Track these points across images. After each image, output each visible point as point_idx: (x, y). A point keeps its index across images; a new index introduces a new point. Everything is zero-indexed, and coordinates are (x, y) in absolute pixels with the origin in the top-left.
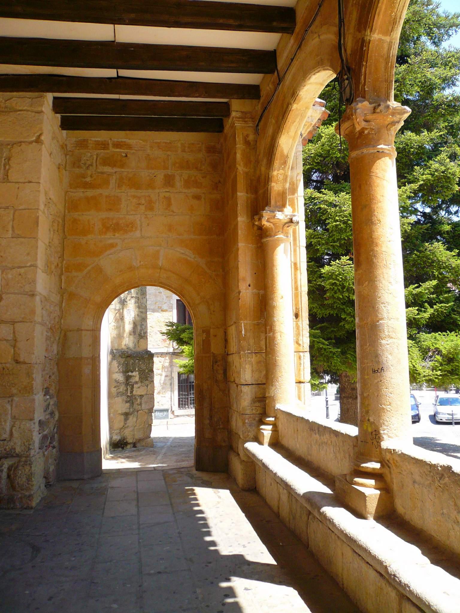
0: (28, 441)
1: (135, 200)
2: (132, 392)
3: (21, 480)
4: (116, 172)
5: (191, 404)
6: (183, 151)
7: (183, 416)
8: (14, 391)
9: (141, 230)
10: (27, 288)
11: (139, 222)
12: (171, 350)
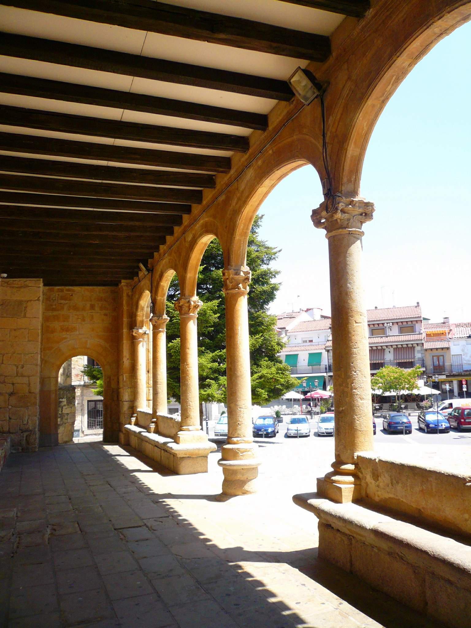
1: (76, 317)
4: (67, 303)
5: (97, 425)
7: (91, 435)
8: (29, 404)
9: (79, 330)
12: (82, 383)
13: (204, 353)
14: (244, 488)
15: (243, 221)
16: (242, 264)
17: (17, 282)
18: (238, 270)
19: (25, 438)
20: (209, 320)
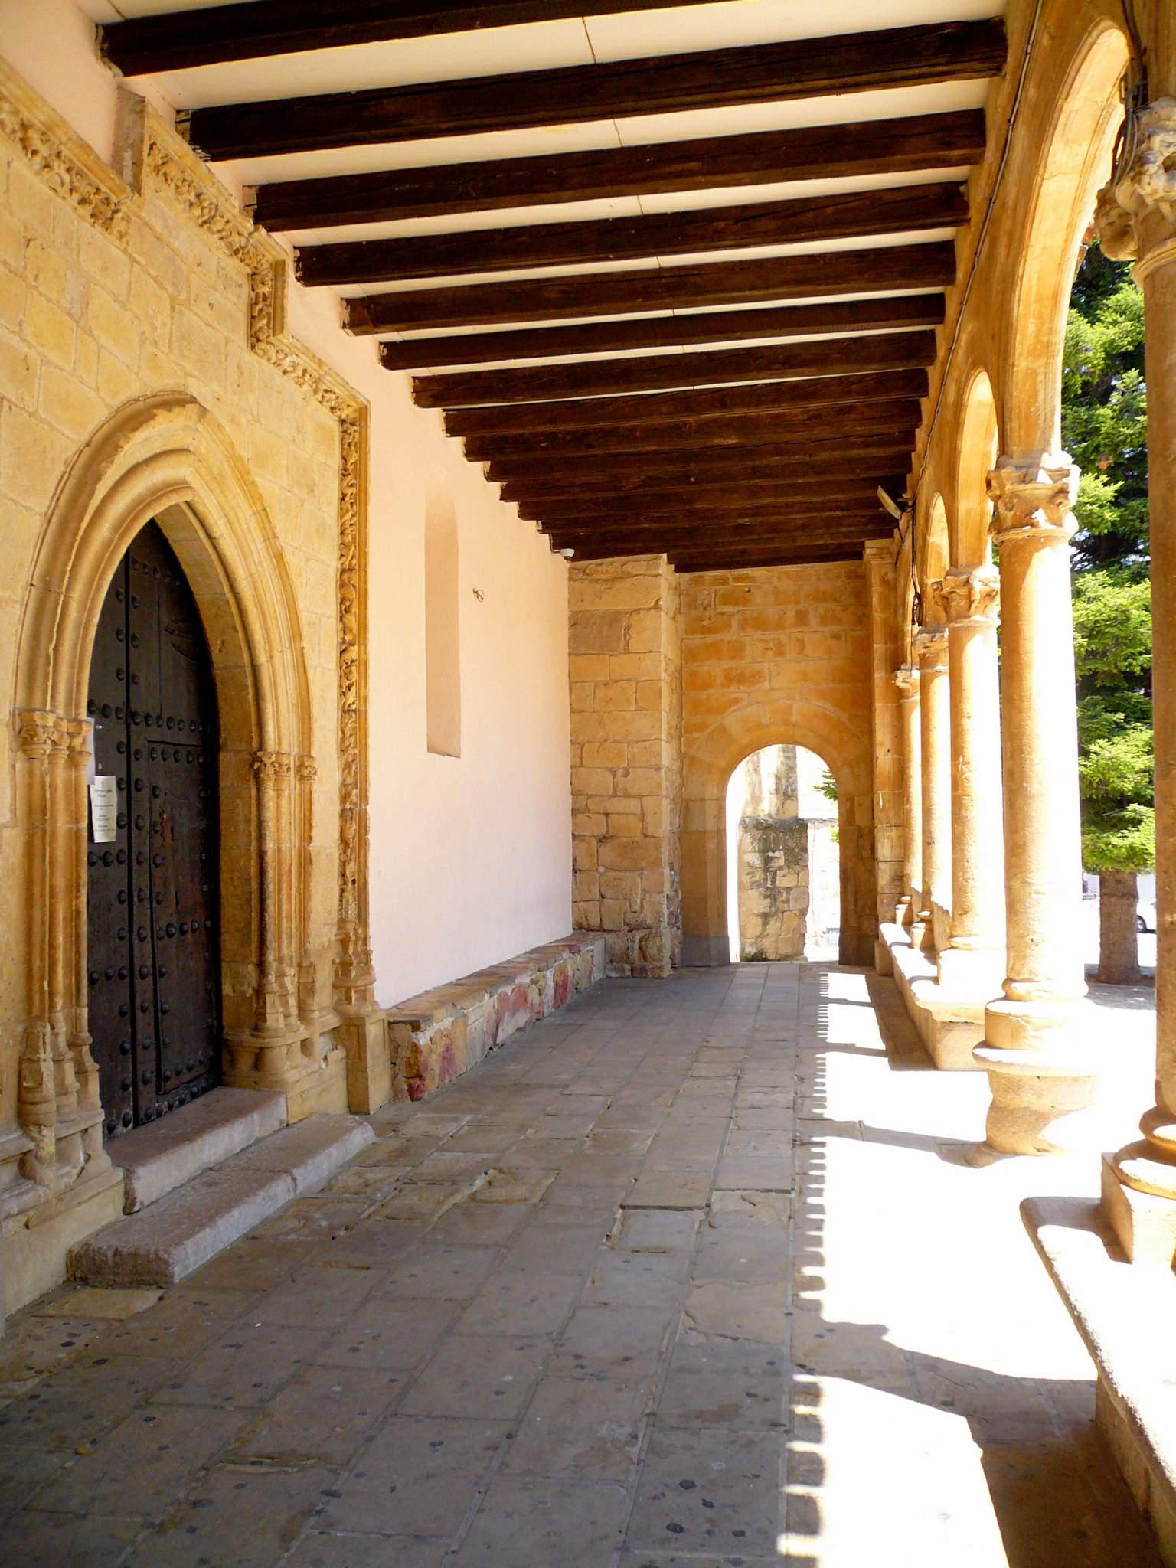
0: (658, 913)
2: (773, 882)
3: (652, 951)
6: (819, 579)
8: (644, 864)
10: (653, 762)
11: (766, 671)
13: (1125, 729)
14: (1040, 1136)
15: (1033, 306)
16: (1045, 448)
17: (605, 567)
18: (1029, 466)
19: (636, 946)
20: (1139, 636)
